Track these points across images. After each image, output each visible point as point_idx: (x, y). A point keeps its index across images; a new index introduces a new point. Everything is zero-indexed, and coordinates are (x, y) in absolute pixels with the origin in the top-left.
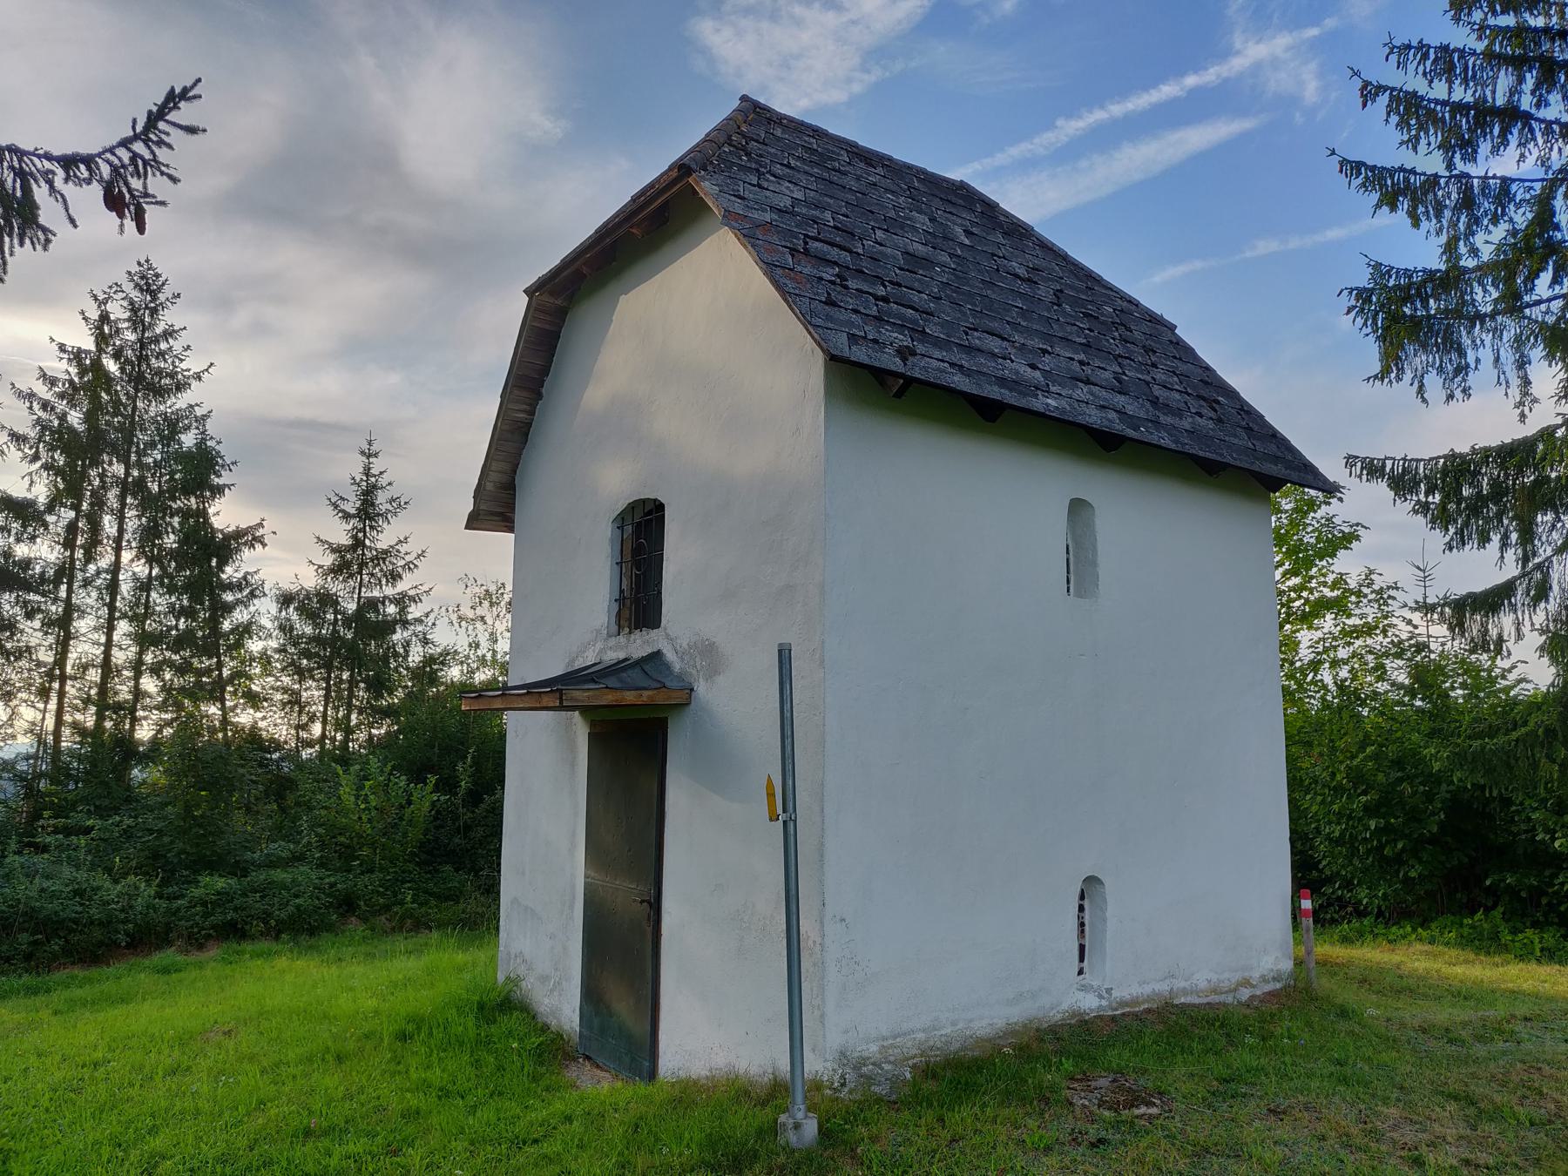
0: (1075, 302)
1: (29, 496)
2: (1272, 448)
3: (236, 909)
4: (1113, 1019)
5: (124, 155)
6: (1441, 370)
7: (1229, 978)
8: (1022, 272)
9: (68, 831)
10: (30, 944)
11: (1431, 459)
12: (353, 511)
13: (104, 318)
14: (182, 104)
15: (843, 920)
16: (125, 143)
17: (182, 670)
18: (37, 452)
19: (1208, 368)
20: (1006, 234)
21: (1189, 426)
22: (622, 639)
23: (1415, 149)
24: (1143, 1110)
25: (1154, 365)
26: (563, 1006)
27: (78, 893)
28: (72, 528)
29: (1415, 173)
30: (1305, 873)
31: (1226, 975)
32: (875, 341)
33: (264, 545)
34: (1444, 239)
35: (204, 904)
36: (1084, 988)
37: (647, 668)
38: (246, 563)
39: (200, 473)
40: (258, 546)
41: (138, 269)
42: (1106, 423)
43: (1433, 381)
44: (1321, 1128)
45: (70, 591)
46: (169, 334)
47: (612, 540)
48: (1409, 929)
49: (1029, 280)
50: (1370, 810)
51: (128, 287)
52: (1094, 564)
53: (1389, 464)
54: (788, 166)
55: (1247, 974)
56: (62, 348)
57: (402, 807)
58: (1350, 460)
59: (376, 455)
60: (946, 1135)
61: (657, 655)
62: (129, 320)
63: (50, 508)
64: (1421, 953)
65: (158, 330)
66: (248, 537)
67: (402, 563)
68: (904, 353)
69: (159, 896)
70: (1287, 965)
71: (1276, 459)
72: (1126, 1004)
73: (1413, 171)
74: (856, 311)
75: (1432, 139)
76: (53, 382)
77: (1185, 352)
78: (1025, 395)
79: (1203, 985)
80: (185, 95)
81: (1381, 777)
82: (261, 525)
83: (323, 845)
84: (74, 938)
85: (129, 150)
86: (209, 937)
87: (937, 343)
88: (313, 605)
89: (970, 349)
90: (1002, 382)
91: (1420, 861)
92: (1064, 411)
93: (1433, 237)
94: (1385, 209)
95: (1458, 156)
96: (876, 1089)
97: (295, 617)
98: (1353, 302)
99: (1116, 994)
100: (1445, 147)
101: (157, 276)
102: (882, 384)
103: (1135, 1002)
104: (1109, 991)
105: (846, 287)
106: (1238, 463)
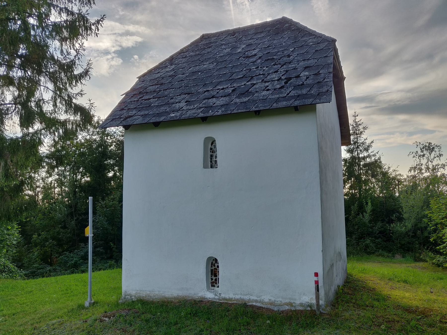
59: (357, 116)
72: (226, 300)
79: (266, 300)
99: (223, 296)
103: (230, 299)
104: (220, 294)
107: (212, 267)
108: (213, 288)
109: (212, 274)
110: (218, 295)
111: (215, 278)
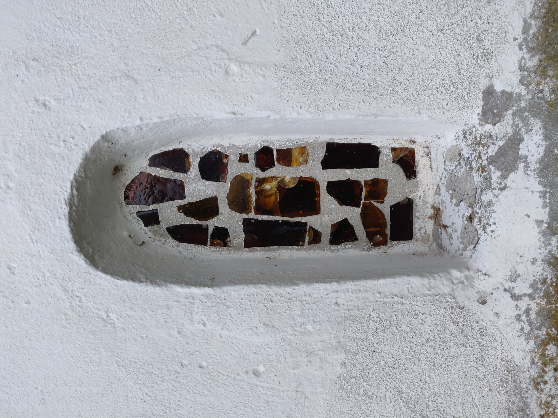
104: (494, 105)
107: (221, 237)
108: (422, 224)
109: (294, 236)
110: (502, 129)
111: (327, 202)
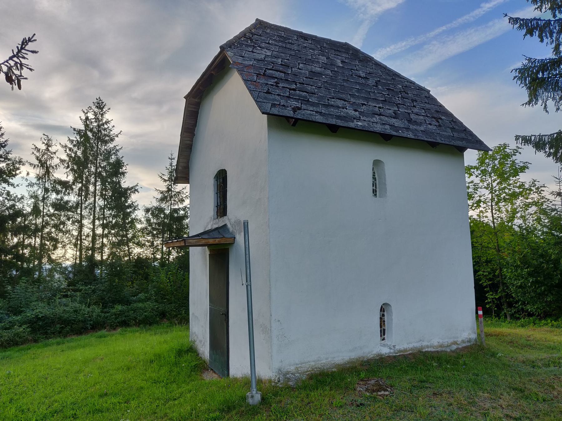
0: (384, 85)
1: (67, 180)
2: (463, 135)
3: (125, 316)
4: (395, 357)
5: (12, 63)
6: (554, 99)
7: (447, 341)
8: (363, 75)
9: (75, 291)
10: (60, 328)
11: (551, 135)
12: (167, 179)
13: (87, 118)
14: (30, 43)
15: (279, 321)
16: (11, 58)
17: (116, 235)
18: (68, 165)
19: (441, 106)
20: (360, 61)
21: (427, 128)
22: (217, 220)
23: (541, 10)
24: (383, 392)
25: (414, 106)
26: (205, 350)
27: (75, 311)
28: (80, 189)
29: (541, 20)
30: (480, 300)
31: (447, 340)
32: (284, 106)
33: (138, 192)
34: (554, 45)
35: (115, 315)
36: (384, 345)
37: (220, 230)
38: (134, 198)
39: (117, 169)
40: (136, 192)
41: (96, 101)
42: (383, 130)
43: (551, 103)
44: (452, 400)
45: (81, 211)
46: (107, 122)
47: (214, 185)
48: (549, 321)
49: (366, 78)
50: (530, 274)
51: (94, 107)
52: (385, 184)
53: (533, 138)
54: (269, 43)
55: (455, 340)
56: (74, 129)
57: (182, 281)
58: (517, 138)
60: (306, 401)
61: (225, 225)
62: (95, 118)
63: (74, 183)
64: (547, 331)
65: (104, 121)
66: (134, 190)
67: (184, 196)
68: (295, 109)
69: (102, 312)
70: (474, 336)
71: (462, 139)
72: (402, 351)
73: (540, 19)
74: (278, 95)
75: (547, 6)
76: (72, 141)
77: (432, 100)
78: (347, 121)
79: (436, 344)
80: (30, 40)
81: (535, 262)
82: (137, 185)
83: (156, 294)
84: (74, 326)
85: (13, 60)
86: (117, 326)
87: (313, 104)
88: (156, 212)
89: (327, 106)
90: (339, 117)
91: (552, 294)
92: (364, 126)
93: (549, 45)
94: (528, 35)
95: (557, 12)
96: (291, 383)
97: (151, 217)
98: (517, 74)
99: (397, 347)
100: (552, 8)
101: (103, 103)
102: (288, 121)
103: (405, 350)
104: (394, 346)
105: (278, 86)
106: (443, 142)
